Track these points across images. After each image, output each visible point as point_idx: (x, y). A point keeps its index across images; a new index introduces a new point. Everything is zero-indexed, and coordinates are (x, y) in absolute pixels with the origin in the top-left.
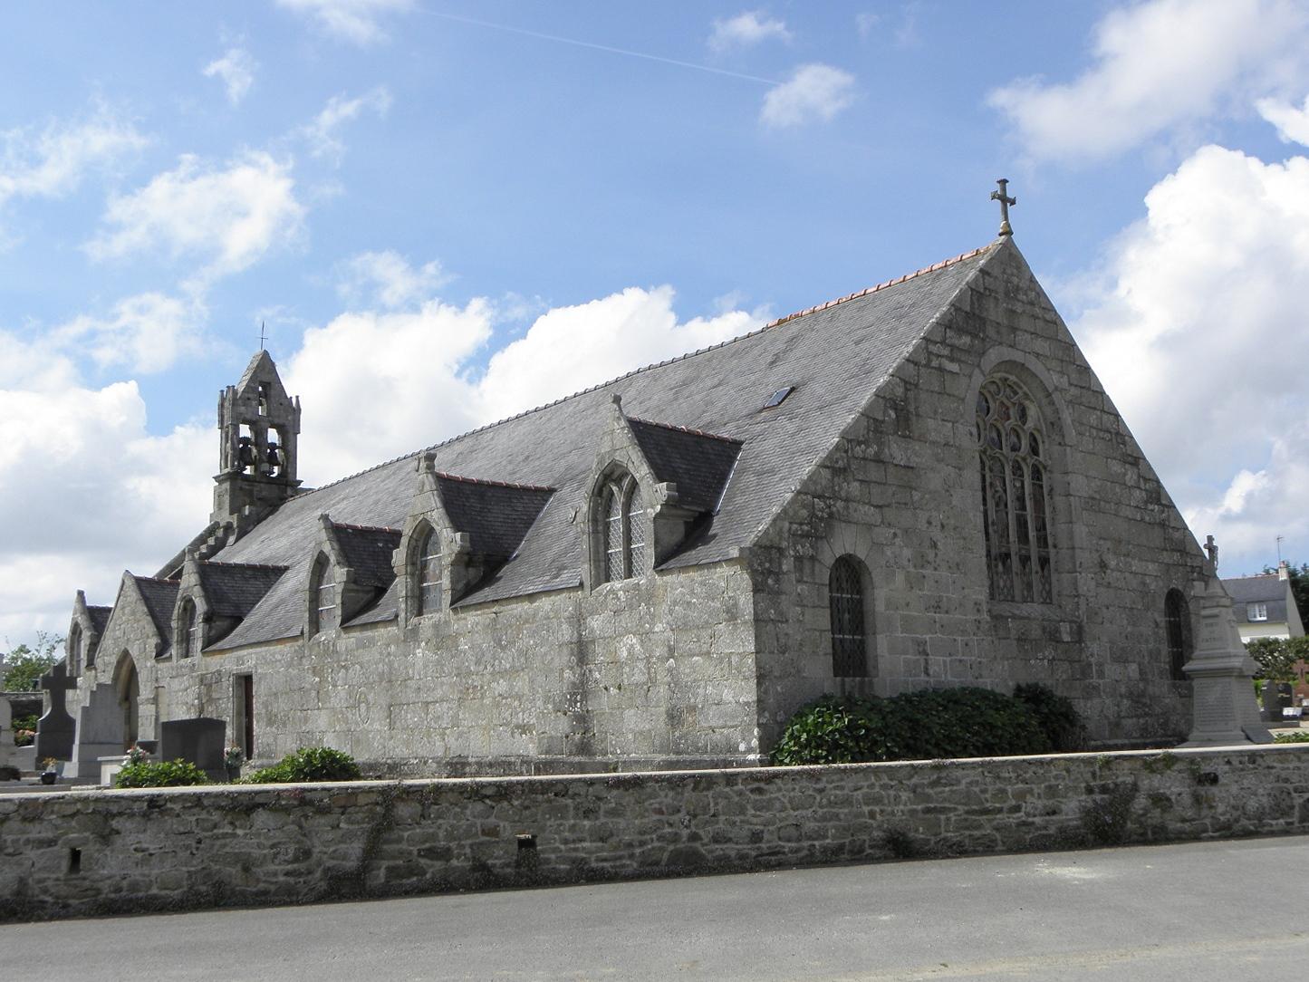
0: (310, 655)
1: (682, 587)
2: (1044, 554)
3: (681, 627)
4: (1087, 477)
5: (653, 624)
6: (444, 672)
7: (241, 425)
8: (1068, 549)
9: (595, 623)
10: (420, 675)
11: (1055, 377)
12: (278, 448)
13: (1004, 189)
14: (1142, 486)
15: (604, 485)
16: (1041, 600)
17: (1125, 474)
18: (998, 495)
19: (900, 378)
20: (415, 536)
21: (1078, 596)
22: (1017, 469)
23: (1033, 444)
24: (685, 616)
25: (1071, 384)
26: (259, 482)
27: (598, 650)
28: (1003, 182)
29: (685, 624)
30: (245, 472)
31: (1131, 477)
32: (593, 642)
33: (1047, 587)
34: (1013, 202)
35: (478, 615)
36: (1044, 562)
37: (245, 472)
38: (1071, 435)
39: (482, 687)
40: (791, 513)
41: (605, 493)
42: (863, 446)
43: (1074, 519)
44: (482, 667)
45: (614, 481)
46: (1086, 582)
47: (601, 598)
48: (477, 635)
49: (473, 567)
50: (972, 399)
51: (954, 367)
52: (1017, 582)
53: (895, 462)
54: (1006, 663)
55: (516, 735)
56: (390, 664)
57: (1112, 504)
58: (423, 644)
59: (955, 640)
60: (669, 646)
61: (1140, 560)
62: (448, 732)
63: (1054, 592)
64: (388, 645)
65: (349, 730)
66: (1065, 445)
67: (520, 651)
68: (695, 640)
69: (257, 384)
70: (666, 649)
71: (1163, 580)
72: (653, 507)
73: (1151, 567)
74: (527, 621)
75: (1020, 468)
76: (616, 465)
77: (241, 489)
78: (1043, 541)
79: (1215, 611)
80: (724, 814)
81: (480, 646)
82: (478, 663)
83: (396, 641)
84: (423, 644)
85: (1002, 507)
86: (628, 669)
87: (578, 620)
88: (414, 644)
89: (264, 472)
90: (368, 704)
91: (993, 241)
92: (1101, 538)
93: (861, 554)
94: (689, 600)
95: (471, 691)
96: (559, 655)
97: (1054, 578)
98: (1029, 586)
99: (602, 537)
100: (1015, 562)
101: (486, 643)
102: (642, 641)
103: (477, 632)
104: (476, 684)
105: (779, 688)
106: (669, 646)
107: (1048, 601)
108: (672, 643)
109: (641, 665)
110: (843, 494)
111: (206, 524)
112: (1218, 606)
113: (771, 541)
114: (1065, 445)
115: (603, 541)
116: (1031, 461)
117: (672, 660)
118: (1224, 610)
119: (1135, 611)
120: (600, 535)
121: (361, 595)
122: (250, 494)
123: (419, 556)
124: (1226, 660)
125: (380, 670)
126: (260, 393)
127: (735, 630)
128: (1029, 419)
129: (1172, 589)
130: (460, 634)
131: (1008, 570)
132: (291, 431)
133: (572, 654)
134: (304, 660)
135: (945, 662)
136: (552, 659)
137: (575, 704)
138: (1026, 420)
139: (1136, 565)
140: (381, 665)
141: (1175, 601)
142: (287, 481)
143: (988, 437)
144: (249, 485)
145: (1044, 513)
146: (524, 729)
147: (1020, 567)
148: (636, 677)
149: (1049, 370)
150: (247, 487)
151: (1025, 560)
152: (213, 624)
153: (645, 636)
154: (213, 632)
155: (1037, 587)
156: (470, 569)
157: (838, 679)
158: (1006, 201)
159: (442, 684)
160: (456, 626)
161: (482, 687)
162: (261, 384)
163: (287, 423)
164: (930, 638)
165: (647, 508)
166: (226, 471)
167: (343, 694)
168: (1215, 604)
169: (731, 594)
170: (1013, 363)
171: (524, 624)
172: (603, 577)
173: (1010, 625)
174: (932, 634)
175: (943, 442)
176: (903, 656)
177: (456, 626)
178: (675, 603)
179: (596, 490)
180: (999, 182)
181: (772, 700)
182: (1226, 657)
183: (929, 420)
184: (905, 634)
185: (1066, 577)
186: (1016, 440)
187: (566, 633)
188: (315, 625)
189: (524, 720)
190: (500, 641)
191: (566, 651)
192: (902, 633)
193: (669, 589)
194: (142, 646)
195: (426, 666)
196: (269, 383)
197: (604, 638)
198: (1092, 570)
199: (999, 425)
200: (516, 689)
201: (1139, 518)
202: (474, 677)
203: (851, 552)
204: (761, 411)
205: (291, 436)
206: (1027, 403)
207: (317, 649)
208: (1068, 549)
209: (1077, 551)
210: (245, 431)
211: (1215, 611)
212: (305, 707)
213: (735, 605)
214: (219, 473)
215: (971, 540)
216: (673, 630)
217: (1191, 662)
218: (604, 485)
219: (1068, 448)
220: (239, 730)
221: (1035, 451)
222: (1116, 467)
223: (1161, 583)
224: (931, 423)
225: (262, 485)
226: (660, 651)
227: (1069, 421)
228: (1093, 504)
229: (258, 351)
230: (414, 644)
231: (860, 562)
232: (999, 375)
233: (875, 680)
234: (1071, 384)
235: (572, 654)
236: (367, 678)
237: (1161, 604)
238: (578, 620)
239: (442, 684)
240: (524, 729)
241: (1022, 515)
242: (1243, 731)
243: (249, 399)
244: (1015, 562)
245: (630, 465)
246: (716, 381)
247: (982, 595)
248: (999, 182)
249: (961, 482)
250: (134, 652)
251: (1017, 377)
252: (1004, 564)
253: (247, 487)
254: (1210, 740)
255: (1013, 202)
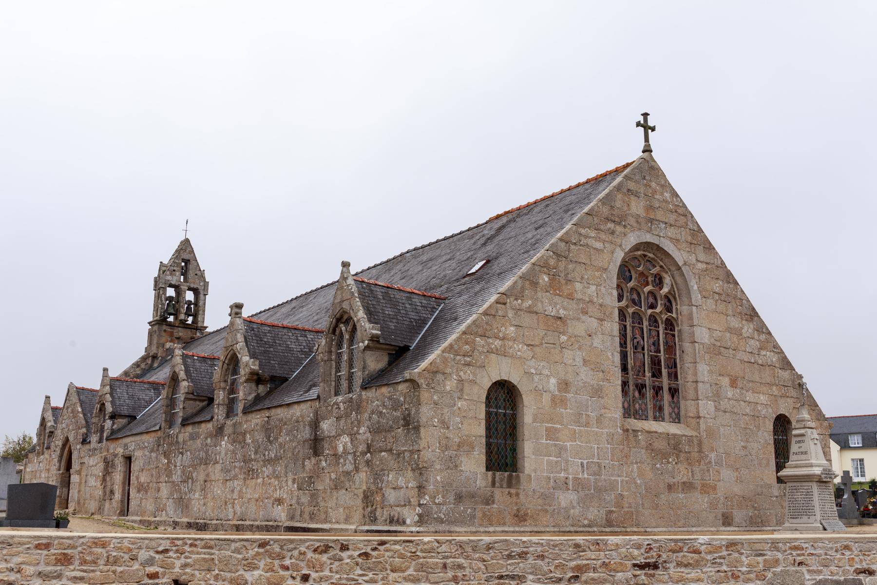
0: (164, 444)
1: (378, 400)
2: (673, 385)
3: (376, 430)
4: (709, 329)
5: (359, 427)
6: (236, 459)
7: (168, 288)
8: (693, 382)
9: (326, 426)
10: (223, 460)
11: (685, 255)
12: (193, 304)
13: (646, 120)
14: (756, 337)
15: (337, 326)
16: (671, 420)
17: (742, 328)
18: (635, 341)
19: (554, 253)
20: (226, 362)
21: (699, 417)
22: (653, 320)
23: (668, 304)
24: (378, 422)
25: (698, 261)
26: (177, 327)
27: (326, 446)
28: (645, 115)
29: (378, 428)
30: (168, 320)
31: (748, 329)
32: (323, 439)
33: (676, 410)
34: (638, 124)
35: (258, 418)
36: (674, 392)
37: (168, 320)
38: (696, 297)
39: (257, 470)
40: (456, 347)
41: (337, 332)
42: (520, 300)
43: (698, 360)
44: (258, 456)
45: (343, 323)
46: (707, 407)
47: (330, 408)
48: (256, 433)
49: (262, 384)
50: (614, 269)
51: (599, 245)
52: (650, 406)
53: (546, 313)
54: (635, 466)
55: (275, 506)
56: (207, 452)
57: (730, 350)
58: (226, 438)
59: (592, 447)
60: (368, 444)
61: (754, 392)
62: (236, 502)
63: (682, 413)
64: (206, 438)
65: (181, 498)
66: (692, 305)
67: (280, 444)
68: (383, 440)
69: (180, 261)
70: (366, 446)
71: (772, 408)
72: (363, 342)
73: (763, 398)
74: (285, 424)
75: (656, 321)
76: (344, 312)
77: (165, 331)
78: (674, 376)
79: (802, 431)
80: (707, 561)
81: (257, 441)
82: (256, 453)
83: (210, 435)
84: (226, 438)
85: (640, 350)
86: (342, 460)
87: (315, 424)
88: (221, 438)
89: (181, 320)
90: (192, 480)
91: (635, 154)
92: (720, 375)
93: (514, 379)
94: (381, 410)
95: (251, 472)
96: (303, 449)
97: (682, 403)
98: (661, 409)
99: (334, 364)
100: (649, 393)
101: (260, 437)
102: (352, 439)
103: (257, 431)
104: (254, 468)
105: (438, 478)
106: (368, 444)
107: (677, 421)
108: (369, 442)
109: (350, 457)
110: (501, 335)
111: (142, 353)
112: (805, 428)
113: (437, 367)
114: (692, 305)
115: (334, 366)
116: (664, 317)
117: (369, 455)
118: (809, 431)
119: (748, 431)
120: (332, 362)
121: (198, 403)
122: (171, 335)
123: (230, 376)
124: (809, 469)
125: (201, 456)
126: (182, 267)
127: (408, 432)
128: (665, 286)
129: (780, 415)
130: (247, 432)
131: (642, 395)
132: (202, 292)
133: (310, 448)
134: (160, 447)
135: (582, 464)
136: (299, 451)
137: (311, 485)
138: (663, 286)
139: (750, 396)
140: (201, 453)
141: (782, 424)
142: (197, 327)
143: (629, 298)
144: (171, 329)
145: (675, 354)
146: (279, 501)
147: (670, 399)
148: (347, 466)
149: (679, 250)
150: (169, 330)
151: (658, 390)
152: (116, 421)
153: (353, 436)
154: (115, 427)
155: (667, 410)
156: (260, 386)
157: (490, 473)
158: (646, 127)
159: (235, 467)
160: (245, 426)
161: (257, 470)
162: (183, 260)
163: (199, 287)
164: (570, 445)
165: (359, 343)
166: (156, 319)
167: (179, 472)
168: (803, 426)
169: (407, 407)
170: (648, 244)
171: (284, 425)
172: (333, 392)
173: (640, 437)
174: (572, 441)
175: (587, 299)
176: (546, 458)
177: (245, 426)
178: (373, 413)
179: (331, 329)
180: (642, 115)
181: (432, 487)
182: (810, 466)
183: (576, 283)
184: (548, 442)
185: (690, 403)
186: (653, 301)
187: (306, 433)
188: (170, 423)
189: (280, 495)
190: (270, 437)
191: (307, 445)
192: (546, 440)
193: (370, 402)
194: (76, 434)
195: (226, 454)
196: (189, 260)
197: (329, 437)
198: (712, 399)
199: (639, 290)
200: (277, 473)
201: (753, 361)
202: (253, 463)
203: (506, 379)
204: (464, 277)
205: (202, 296)
206: (664, 275)
207: (167, 439)
208: (693, 382)
209: (700, 385)
210: (171, 292)
211: (802, 431)
212: (159, 481)
213: (409, 415)
214: (151, 319)
215: (609, 373)
216: (370, 432)
217: (784, 469)
218: (337, 326)
219: (694, 308)
220: (123, 495)
221: (669, 310)
222: (735, 323)
223: (770, 410)
224: (578, 286)
225: (180, 329)
226: (362, 448)
227: (696, 287)
228: (716, 350)
229: (183, 238)
230: (221, 438)
231: (514, 386)
232: (639, 253)
233: (521, 475)
234: (698, 261)
235: (310, 448)
236: (193, 461)
237: (770, 426)
238: (315, 424)
239: (235, 467)
240: (279, 501)
241: (657, 356)
242: (821, 524)
243: (174, 271)
244: (649, 393)
245: (351, 312)
246: (448, 257)
247: (618, 414)
248: (642, 115)
249: (602, 330)
250: (71, 439)
251: (653, 254)
252: (640, 392)
253: (169, 330)
254: (796, 530)
255: (638, 124)
